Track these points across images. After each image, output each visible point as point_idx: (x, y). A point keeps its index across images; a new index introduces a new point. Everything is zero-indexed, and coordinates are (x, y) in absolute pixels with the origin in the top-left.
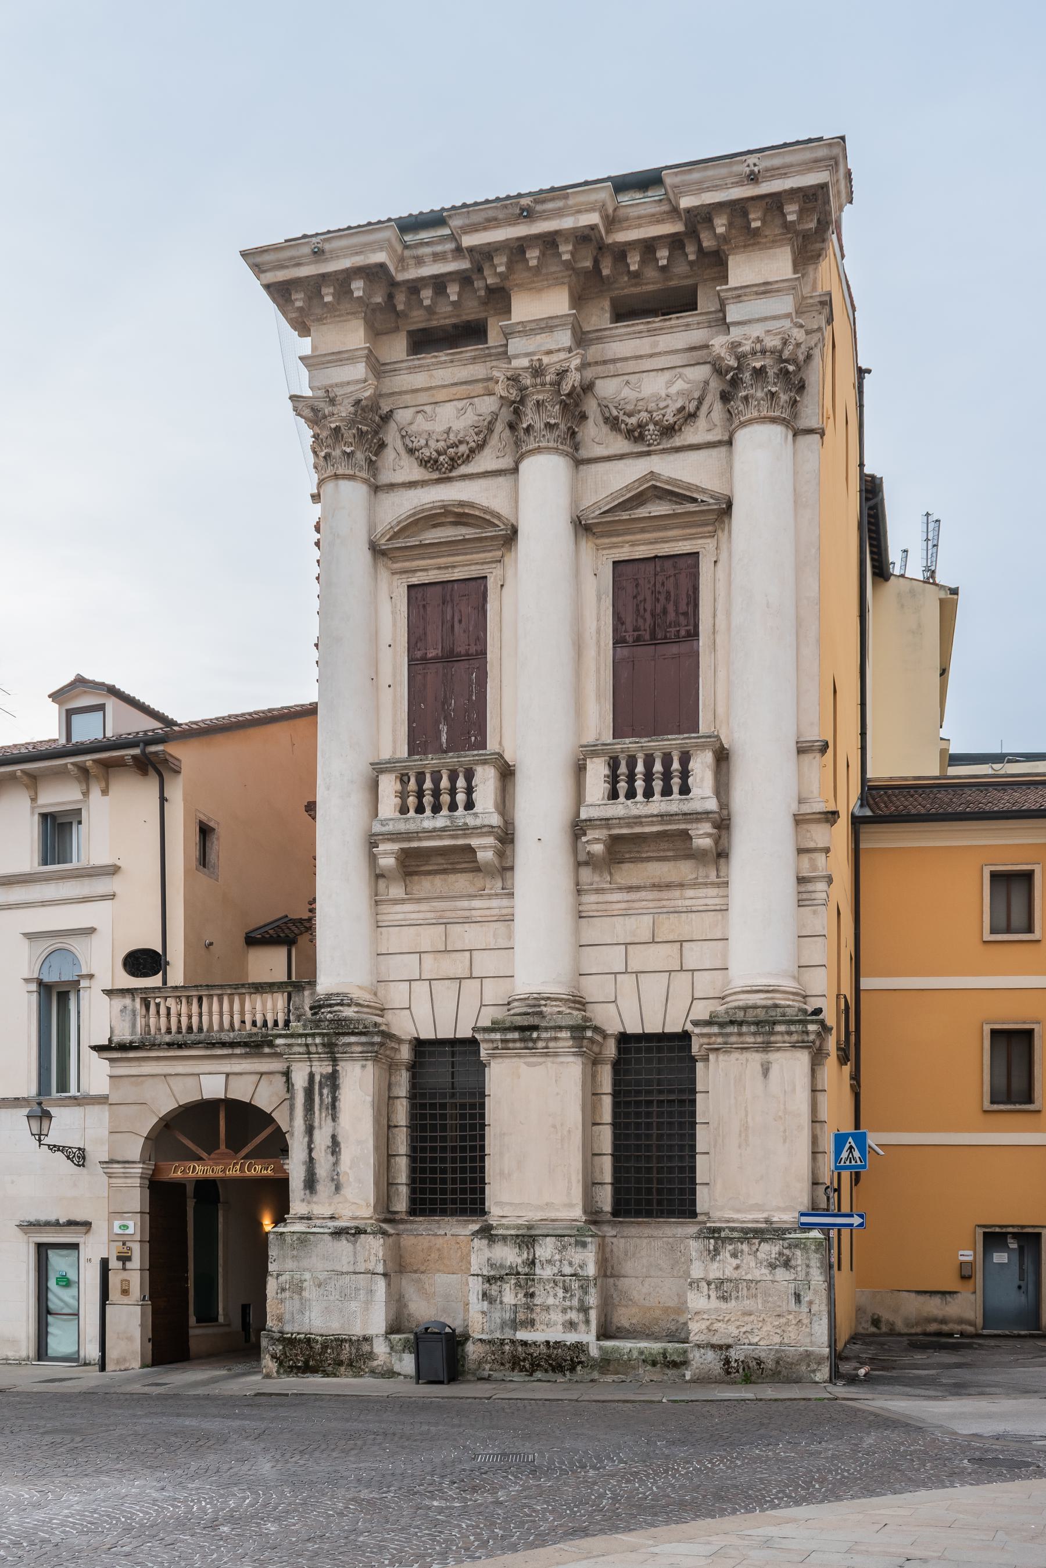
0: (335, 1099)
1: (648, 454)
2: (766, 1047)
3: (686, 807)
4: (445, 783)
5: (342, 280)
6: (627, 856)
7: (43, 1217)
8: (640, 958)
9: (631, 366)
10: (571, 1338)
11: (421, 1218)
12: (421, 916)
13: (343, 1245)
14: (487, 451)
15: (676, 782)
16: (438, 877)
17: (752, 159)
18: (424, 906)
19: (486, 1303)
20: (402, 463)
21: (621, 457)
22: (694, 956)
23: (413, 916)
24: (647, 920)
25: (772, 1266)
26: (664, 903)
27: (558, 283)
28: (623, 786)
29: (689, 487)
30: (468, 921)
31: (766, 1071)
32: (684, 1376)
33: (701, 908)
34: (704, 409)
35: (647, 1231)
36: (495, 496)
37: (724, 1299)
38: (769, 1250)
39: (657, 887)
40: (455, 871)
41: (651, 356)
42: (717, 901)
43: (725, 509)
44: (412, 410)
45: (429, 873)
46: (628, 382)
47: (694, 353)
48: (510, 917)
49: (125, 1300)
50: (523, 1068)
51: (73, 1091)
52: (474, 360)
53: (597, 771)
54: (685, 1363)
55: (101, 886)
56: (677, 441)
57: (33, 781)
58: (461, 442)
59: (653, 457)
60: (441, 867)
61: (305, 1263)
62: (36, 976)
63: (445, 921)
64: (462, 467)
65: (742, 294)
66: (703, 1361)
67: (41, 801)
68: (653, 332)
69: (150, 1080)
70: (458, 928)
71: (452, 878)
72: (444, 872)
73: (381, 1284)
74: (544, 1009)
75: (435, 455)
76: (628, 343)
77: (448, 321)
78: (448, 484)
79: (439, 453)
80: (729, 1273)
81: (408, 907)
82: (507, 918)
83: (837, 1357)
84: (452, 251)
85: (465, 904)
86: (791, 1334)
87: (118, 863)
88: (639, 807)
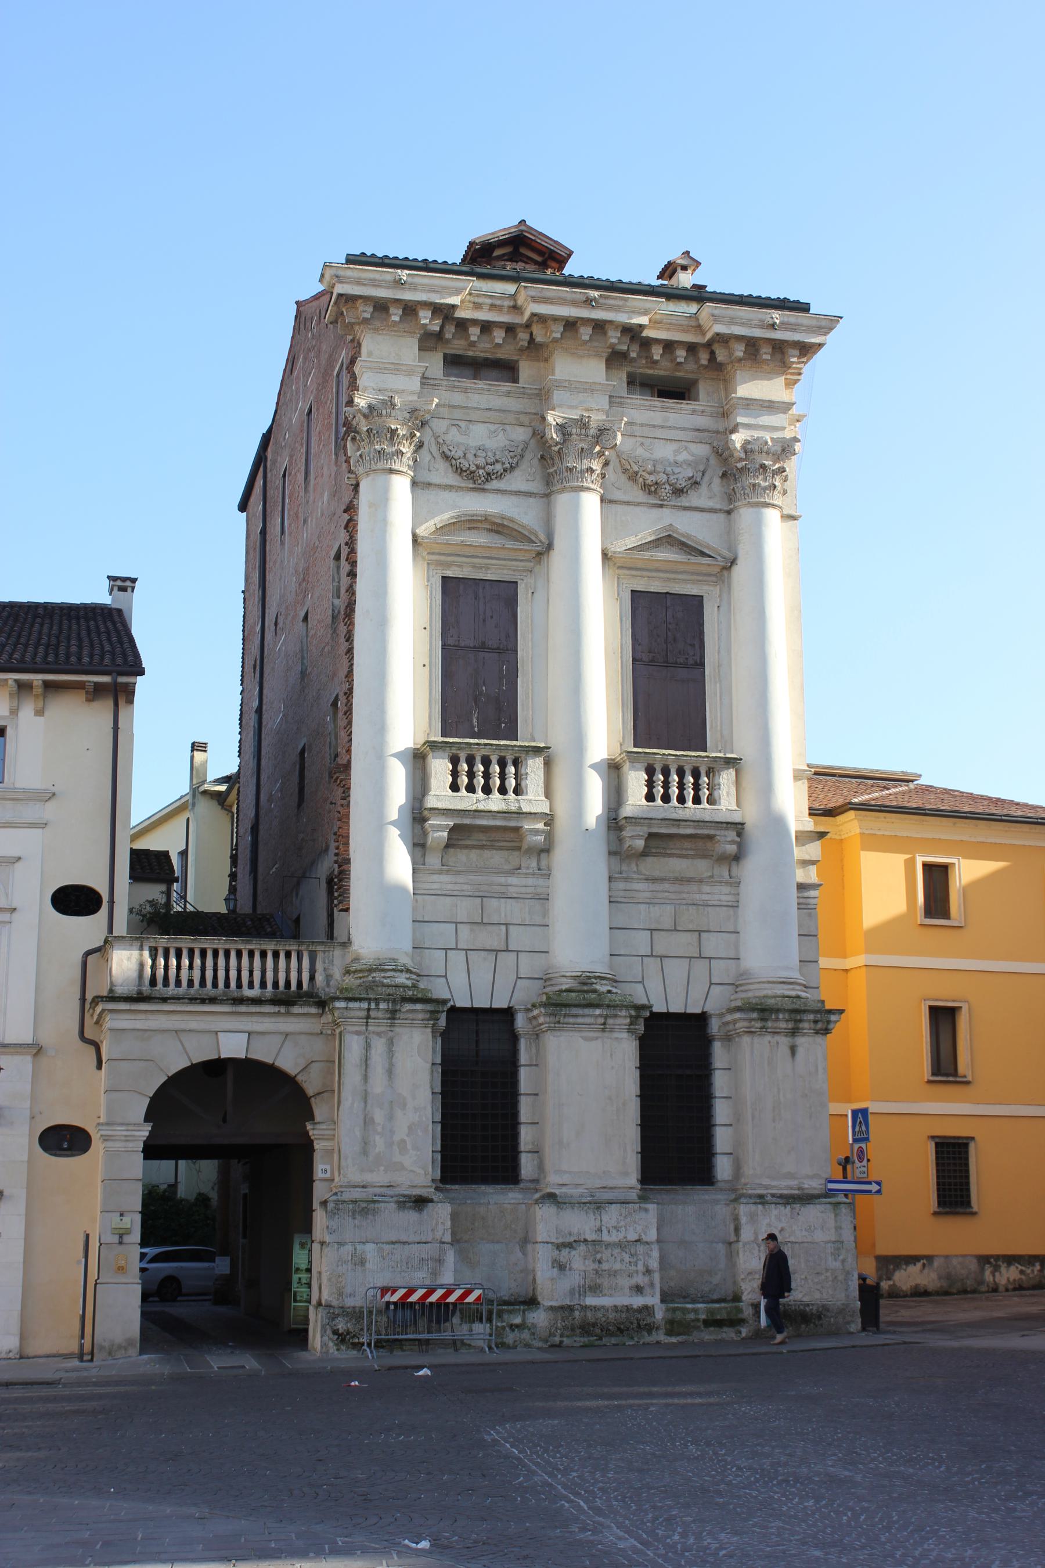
1: (661, 506)
6: (654, 851)
10: (638, 1301)
11: (457, 1187)
12: (457, 887)
14: (517, 473)
16: (474, 851)
18: (460, 879)
19: (555, 1270)
20: (437, 466)
21: (639, 504)
22: (713, 944)
23: (450, 886)
24: (670, 909)
26: (684, 896)
29: (708, 547)
30: (503, 896)
31: (793, 1050)
32: (740, 1333)
33: (715, 903)
34: (706, 478)
36: (526, 514)
40: (492, 848)
41: (663, 427)
42: (730, 898)
44: (446, 423)
45: (467, 847)
46: (642, 444)
47: (697, 433)
48: (545, 896)
52: (508, 394)
55: (31, 812)
56: (684, 501)
58: (497, 461)
59: (664, 509)
60: (480, 843)
63: (481, 894)
64: (495, 482)
70: (494, 902)
71: (487, 853)
72: (482, 847)
74: (598, 987)
75: (473, 468)
77: (482, 355)
78: (482, 494)
79: (478, 467)
81: (444, 878)
82: (542, 896)
84: (509, 307)
85: (502, 880)
87: (54, 789)
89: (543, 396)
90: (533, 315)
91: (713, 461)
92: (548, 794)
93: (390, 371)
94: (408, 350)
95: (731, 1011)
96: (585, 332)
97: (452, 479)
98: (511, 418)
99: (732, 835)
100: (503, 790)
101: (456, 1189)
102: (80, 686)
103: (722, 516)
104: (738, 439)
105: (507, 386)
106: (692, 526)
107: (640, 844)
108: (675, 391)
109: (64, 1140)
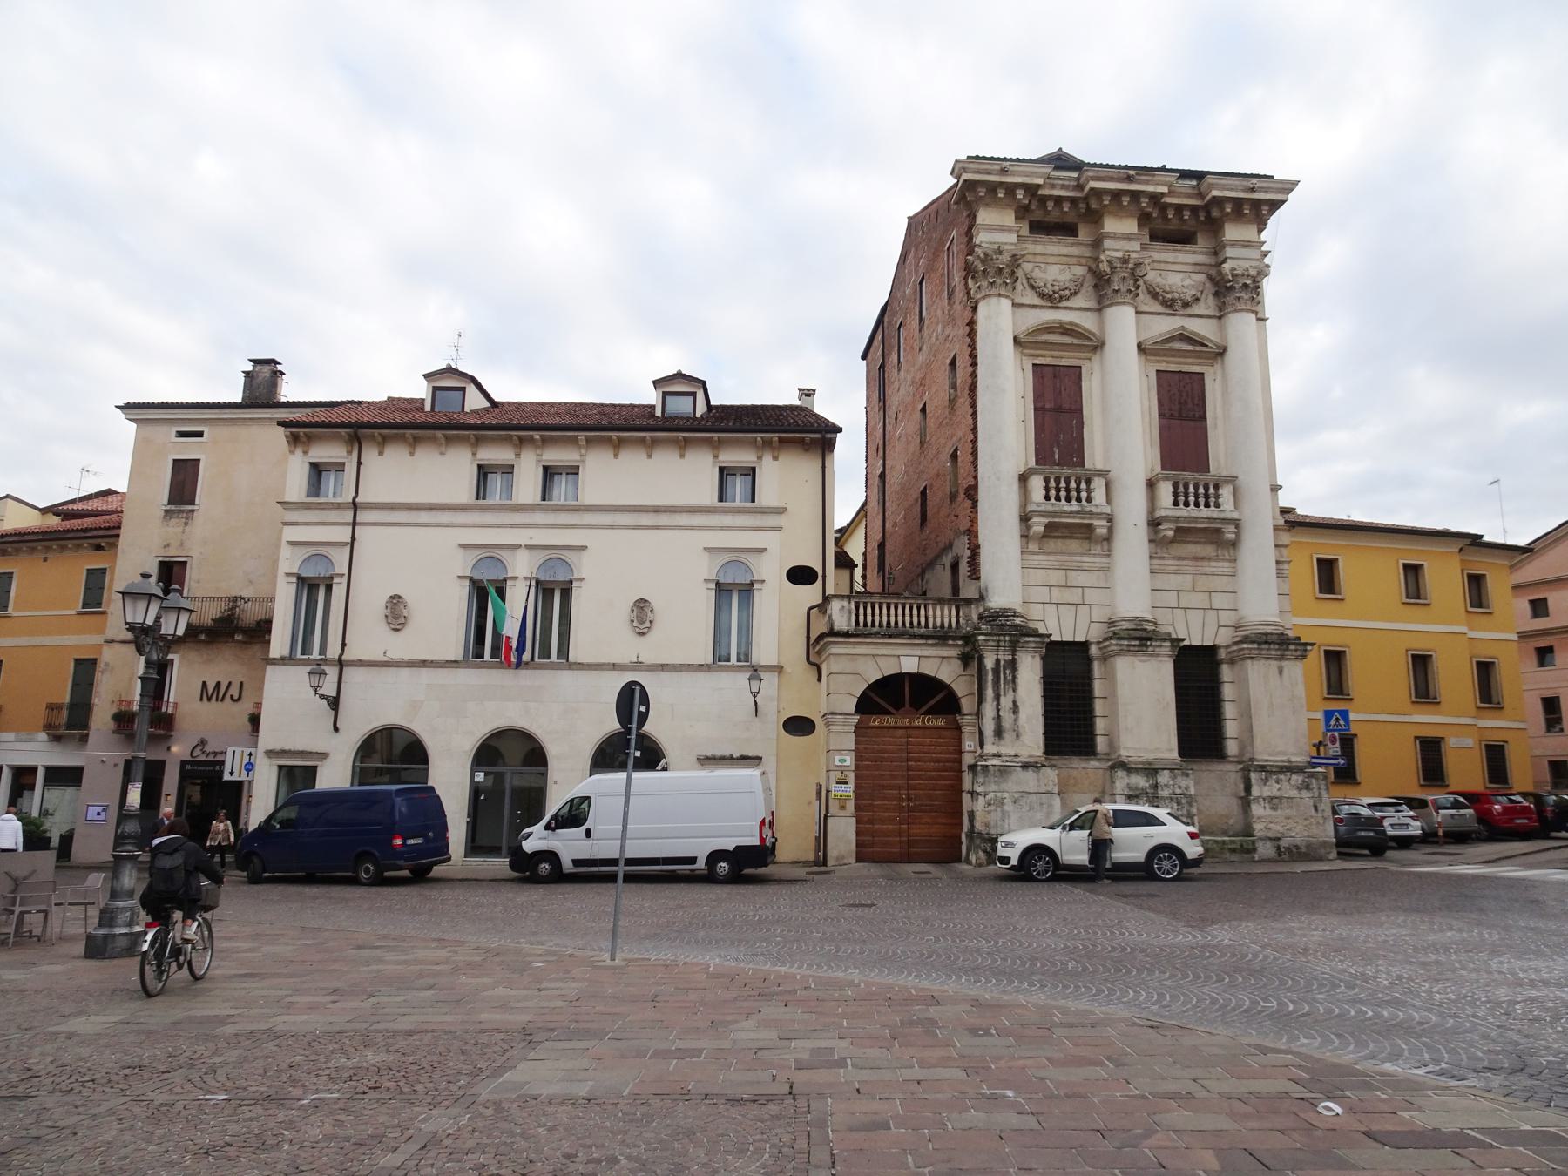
0: (1014, 677)
2: (1281, 658)
3: (1215, 515)
4: (1073, 485)
5: (1011, 189)
7: (718, 753)
8: (1186, 600)
9: (1163, 266)
13: (1030, 773)
15: (1212, 500)
17: (1254, 181)
18: (1052, 558)
21: (1034, 306)
22: (1219, 601)
24: (1189, 577)
25: (1299, 789)
27: (1131, 216)
28: (1182, 499)
29: (1203, 337)
31: (1281, 672)
35: (1204, 767)
37: (1273, 808)
38: (1297, 779)
39: (1196, 559)
43: (1221, 353)
49: (842, 813)
50: (1138, 663)
51: (316, 655)
53: (1037, 484)
54: (1255, 850)
55: (771, 520)
56: (1189, 311)
57: (477, 443)
61: (1004, 786)
62: (468, 574)
65: (1234, 243)
66: (1265, 850)
67: (479, 456)
68: (1175, 251)
69: (862, 659)
71: (1068, 541)
73: (1057, 801)
76: (1162, 253)
80: (1275, 793)
81: (1041, 557)
83: (1338, 845)
86: (1314, 831)
88: (1191, 511)
89: (1097, 244)
90: (1092, 189)
91: (1208, 285)
92: (1109, 501)
93: (997, 229)
94: (1008, 218)
95: (1106, 639)
96: (1126, 200)
97: (1037, 301)
98: (1074, 260)
99: (1232, 528)
100: (1079, 500)
101: (1056, 760)
102: (802, 442)
103: (1215, 321)
104: (1227, 267)
105: (1071, 239)
106: (1201, 328)
107: (1171, 533)
108: (1183, 238)
109: (799, 726)
